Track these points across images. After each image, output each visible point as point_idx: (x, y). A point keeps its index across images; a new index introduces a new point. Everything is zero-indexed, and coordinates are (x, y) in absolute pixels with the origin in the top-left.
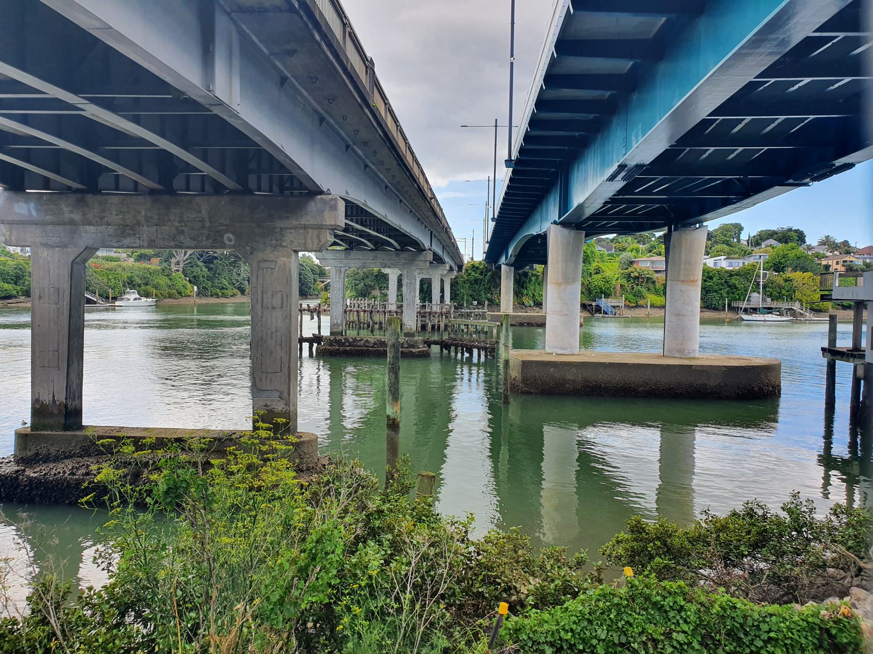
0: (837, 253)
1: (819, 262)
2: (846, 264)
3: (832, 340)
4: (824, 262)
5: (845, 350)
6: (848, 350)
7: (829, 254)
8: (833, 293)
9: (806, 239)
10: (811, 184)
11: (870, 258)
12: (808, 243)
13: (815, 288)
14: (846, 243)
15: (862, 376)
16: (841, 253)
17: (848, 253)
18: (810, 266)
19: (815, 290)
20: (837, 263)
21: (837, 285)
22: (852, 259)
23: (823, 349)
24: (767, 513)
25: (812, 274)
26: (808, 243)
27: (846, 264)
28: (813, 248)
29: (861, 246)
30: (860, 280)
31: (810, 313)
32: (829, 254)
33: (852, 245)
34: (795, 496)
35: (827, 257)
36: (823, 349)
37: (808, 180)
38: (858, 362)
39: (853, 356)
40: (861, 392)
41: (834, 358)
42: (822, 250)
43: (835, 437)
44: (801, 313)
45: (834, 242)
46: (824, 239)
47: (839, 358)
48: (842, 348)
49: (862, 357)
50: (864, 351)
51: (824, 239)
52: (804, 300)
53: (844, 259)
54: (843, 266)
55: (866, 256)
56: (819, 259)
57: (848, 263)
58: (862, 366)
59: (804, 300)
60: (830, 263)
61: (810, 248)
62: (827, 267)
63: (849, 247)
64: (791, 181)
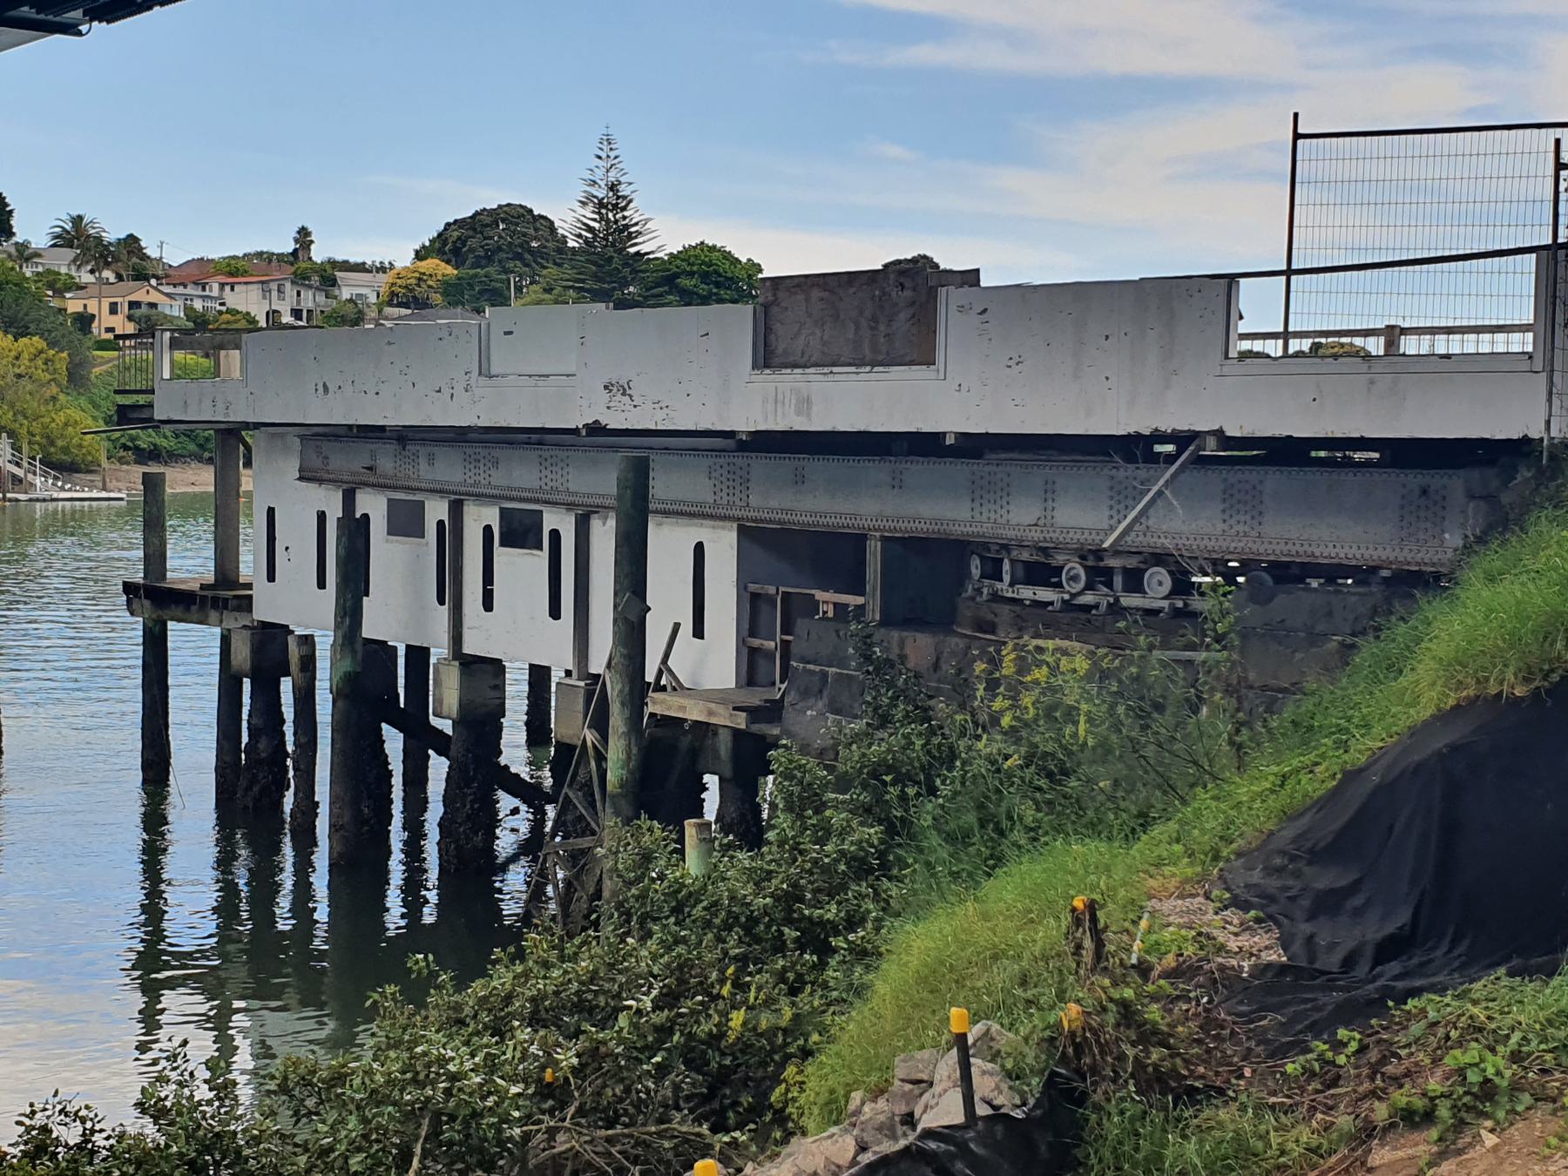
0: (108, 274)
1: (56, 303)
2: (137, 312)
3: (155, 559)
4: (74, 305)
5: (195, 586)
6: (203, 587)
7: (86, 277)
8: (157, 399)
9: (16, 223)
10: (84, 28)
11: (204, 298)
12: (19, 238)
13: (54, 389)
14: (132, 241)
15: (247, 666)
16: (120, 277)
17: (141, 276)
18: (33, 315)
19: (54, 399)
20: (113, 309)
21: (166, 375)
22: (154, 297)
23: (129, 588)
24: (93, 1132)
25: (42, 344)
26: (19, 238)
27: (137, 312)
28: (37, 254)
29: (175, 257)
30: (232, 360)
31: (45, 475)
32: (86, 277)
33: (152, 252)
34: (175, 1056)
35: (81, 288)
36: (129, 588)
37: (77, 14)
38: (234, 621)
39: (220, 605)
40: (245, 716)
41: (164, 614)
42: (62, 263)
43: (172, 866)
44: (14, 476)
45: (99, 239)
46: (68, 227)
47: (179, 612)
48: (183, 581)
49: (246, 604)
50: (249, 586)
51: (68, 227)
52: (24, 431)
53: (133, 298)
54: (130, 318)
55: (190, 290)
56: (59, 293)
57: (144, 310)
58: (247, 633)
59: (24, 431)
60: (92, 308)
61: (25, 254)
62: (84, 321)
63: (145, 257)
64: (26, 11)
